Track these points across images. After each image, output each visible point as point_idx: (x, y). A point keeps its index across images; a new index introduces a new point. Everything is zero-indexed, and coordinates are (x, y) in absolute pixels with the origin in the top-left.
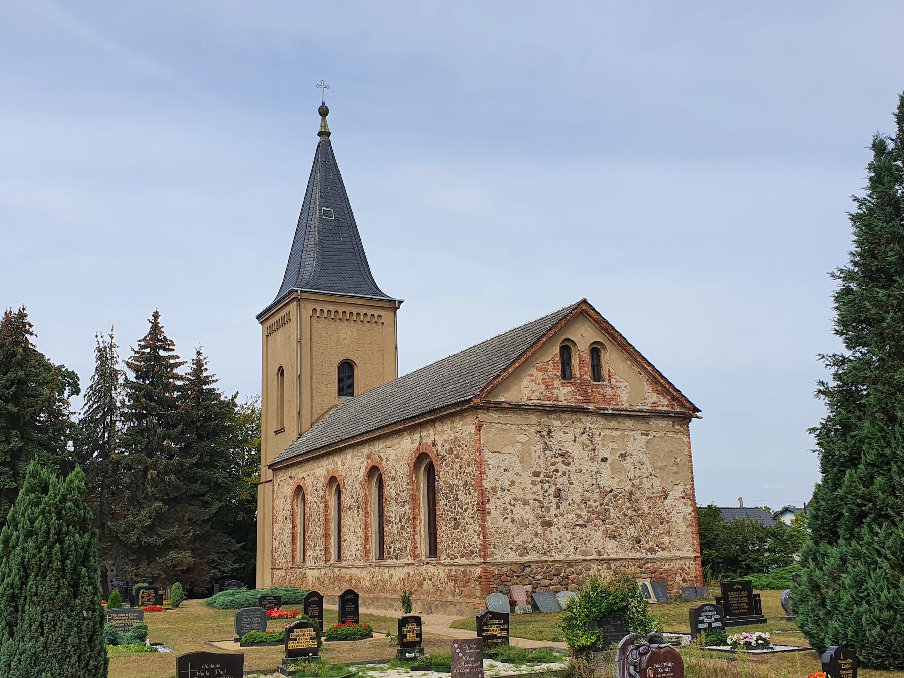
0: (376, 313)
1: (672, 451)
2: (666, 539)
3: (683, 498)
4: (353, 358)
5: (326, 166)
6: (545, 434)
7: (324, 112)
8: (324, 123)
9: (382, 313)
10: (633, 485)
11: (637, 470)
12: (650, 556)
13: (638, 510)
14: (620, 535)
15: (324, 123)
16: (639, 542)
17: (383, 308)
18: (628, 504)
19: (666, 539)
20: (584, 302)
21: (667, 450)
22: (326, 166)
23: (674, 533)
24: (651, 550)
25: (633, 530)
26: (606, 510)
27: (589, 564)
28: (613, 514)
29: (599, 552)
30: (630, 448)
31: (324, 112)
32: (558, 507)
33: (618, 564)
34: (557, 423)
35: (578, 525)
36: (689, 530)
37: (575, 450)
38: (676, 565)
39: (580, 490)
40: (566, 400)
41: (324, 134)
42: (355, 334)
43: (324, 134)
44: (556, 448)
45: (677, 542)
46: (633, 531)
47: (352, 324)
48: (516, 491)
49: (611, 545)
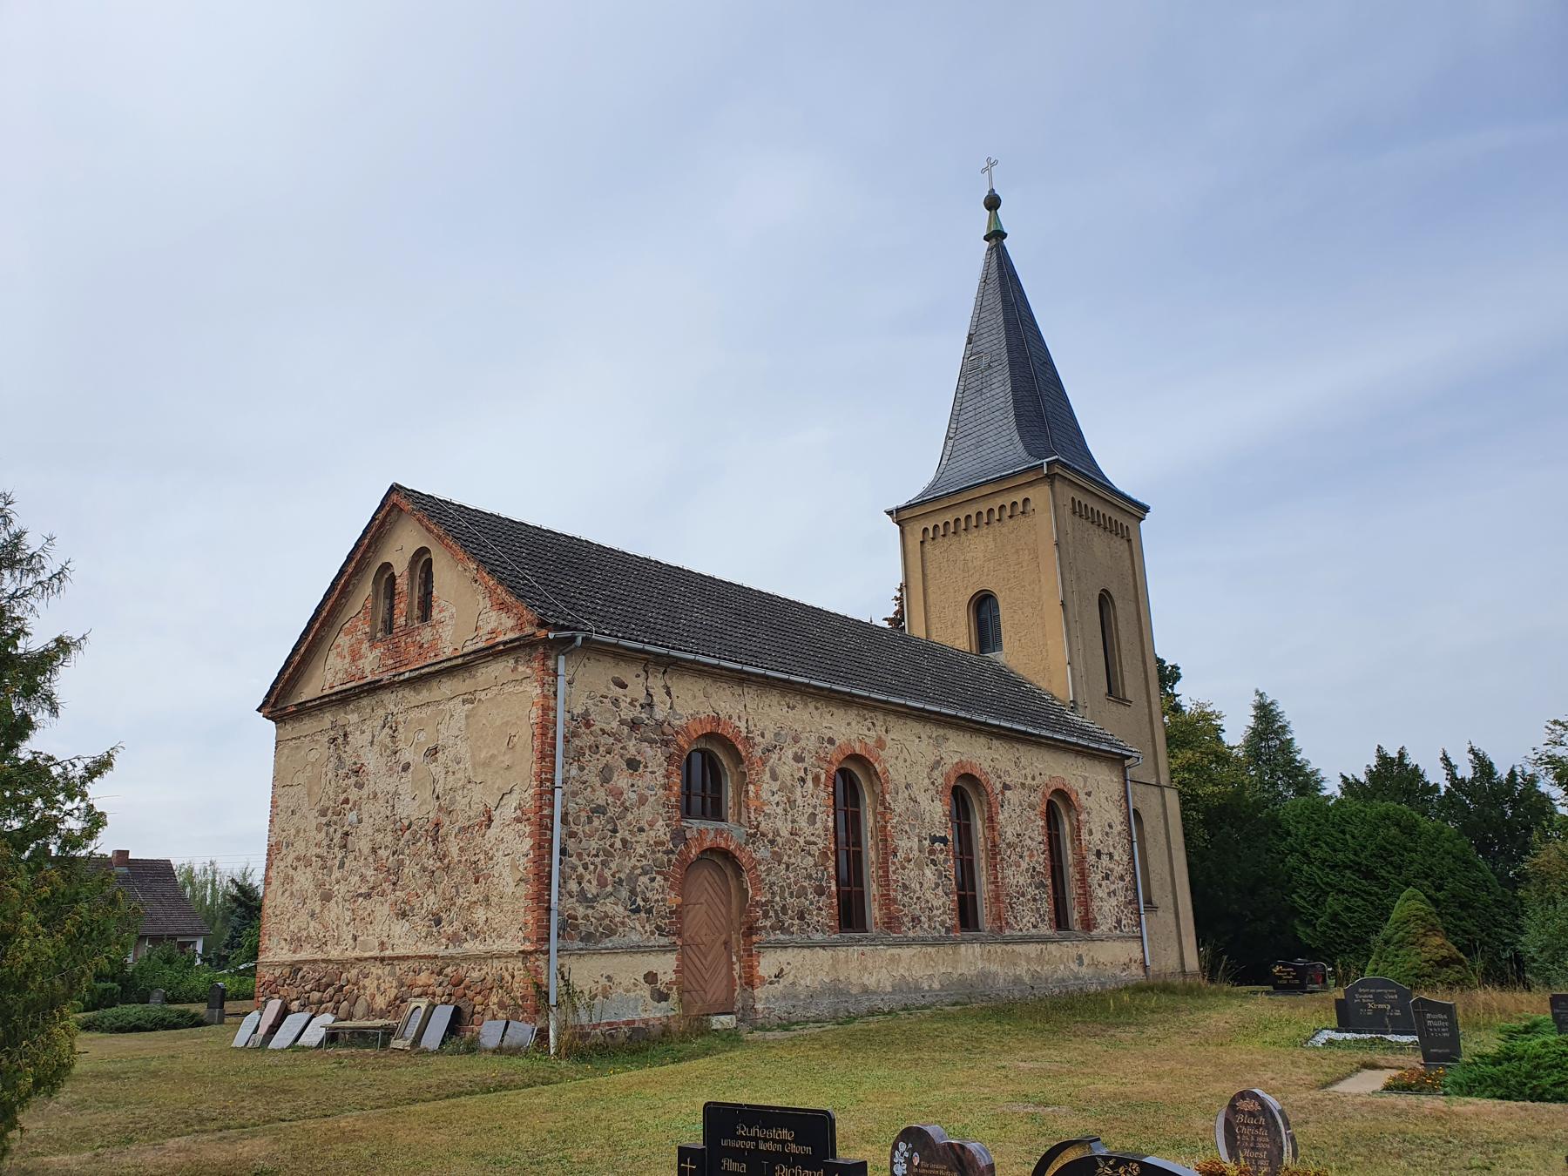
0: (1018, 497)
1: (507, 723)
2: (480, 914)
3: (518, 820)
4: (971, 592)
5: (1003, 282)
6: (340, 740)
7: (993, 203)
8: (994, 219)
9: (1029, 493)
10: (440, 808)
11: (450, 778)
12: (452, 951)
13: (445, 856)
14: (412, 909)
15: (994, 219)
16: (438, 922)
17: (1030, 484)
18: (430, 848)
19: (480, 914)
20: (395, 489)
21: (498, 722)
22: (1003, 282)
23: (494, 900)
24: (454, 939)
25: (432, 898)
26: (401, 863)
27: (368, 965)
28: (410, 869)
29: (382, 943)
30: (445, 736)
31: (993, 203)
32: (342, 865)
33: (405, 966)
34: (354, 718)
35: (360, 895)
36: (522, 890)
37: (372, 761)
38: (491, 969)
39: (370, 832)
40: (372, 671)
41: (996, 236)
42: (991, 545)
43: (996, 236)
44: (349, 761)
45: (498, 919)
46: (432, 901)
47: (984, 530)
48: (300, 847)
49: (400, 928)
